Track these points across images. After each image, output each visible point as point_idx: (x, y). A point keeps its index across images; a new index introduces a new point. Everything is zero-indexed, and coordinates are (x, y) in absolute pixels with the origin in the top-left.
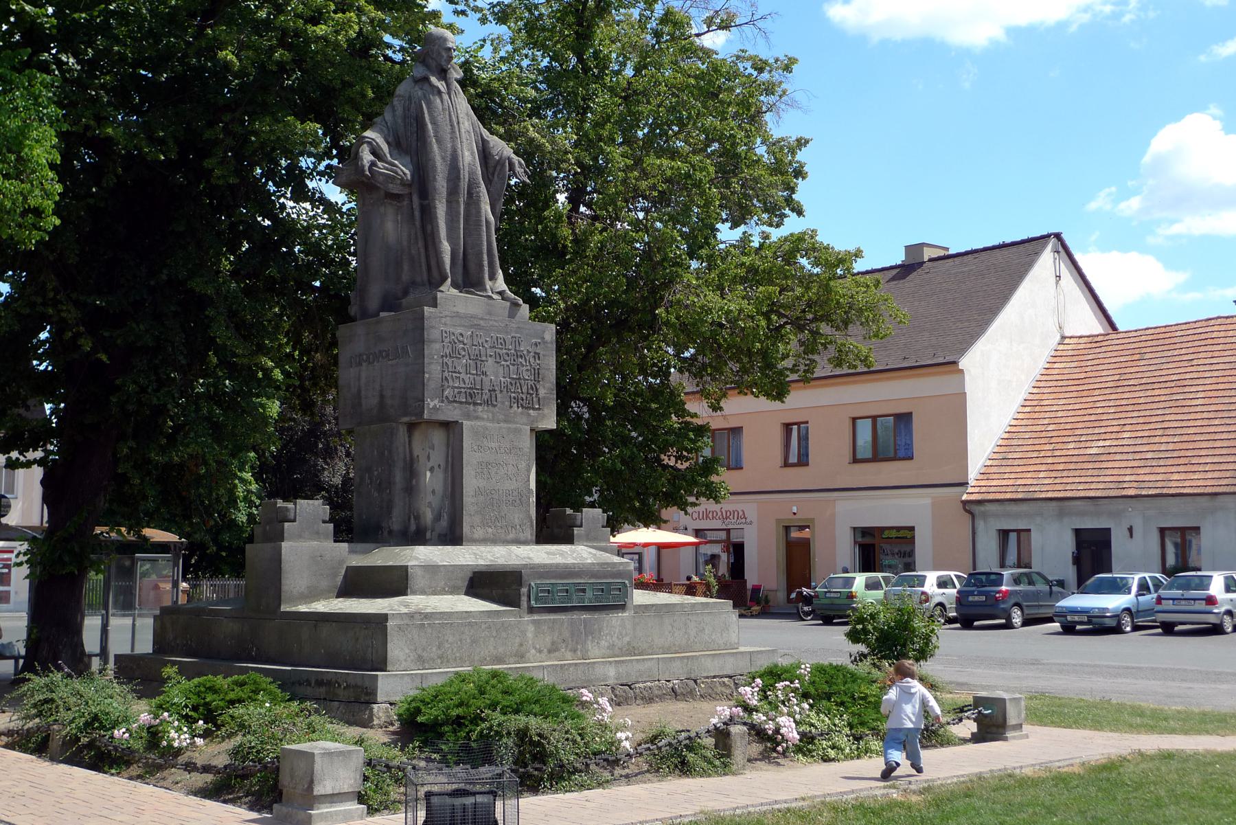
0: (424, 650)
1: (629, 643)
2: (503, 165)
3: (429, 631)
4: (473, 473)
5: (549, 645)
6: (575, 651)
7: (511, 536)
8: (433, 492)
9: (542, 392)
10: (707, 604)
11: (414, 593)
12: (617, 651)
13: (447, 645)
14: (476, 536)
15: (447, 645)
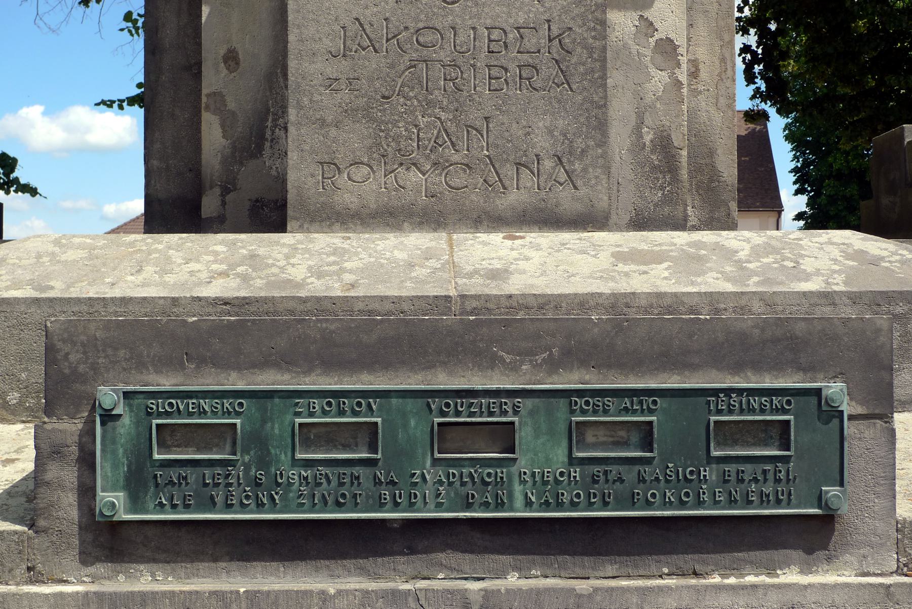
7: (514, 198)
8: (231, 59)
14: (347, 198)
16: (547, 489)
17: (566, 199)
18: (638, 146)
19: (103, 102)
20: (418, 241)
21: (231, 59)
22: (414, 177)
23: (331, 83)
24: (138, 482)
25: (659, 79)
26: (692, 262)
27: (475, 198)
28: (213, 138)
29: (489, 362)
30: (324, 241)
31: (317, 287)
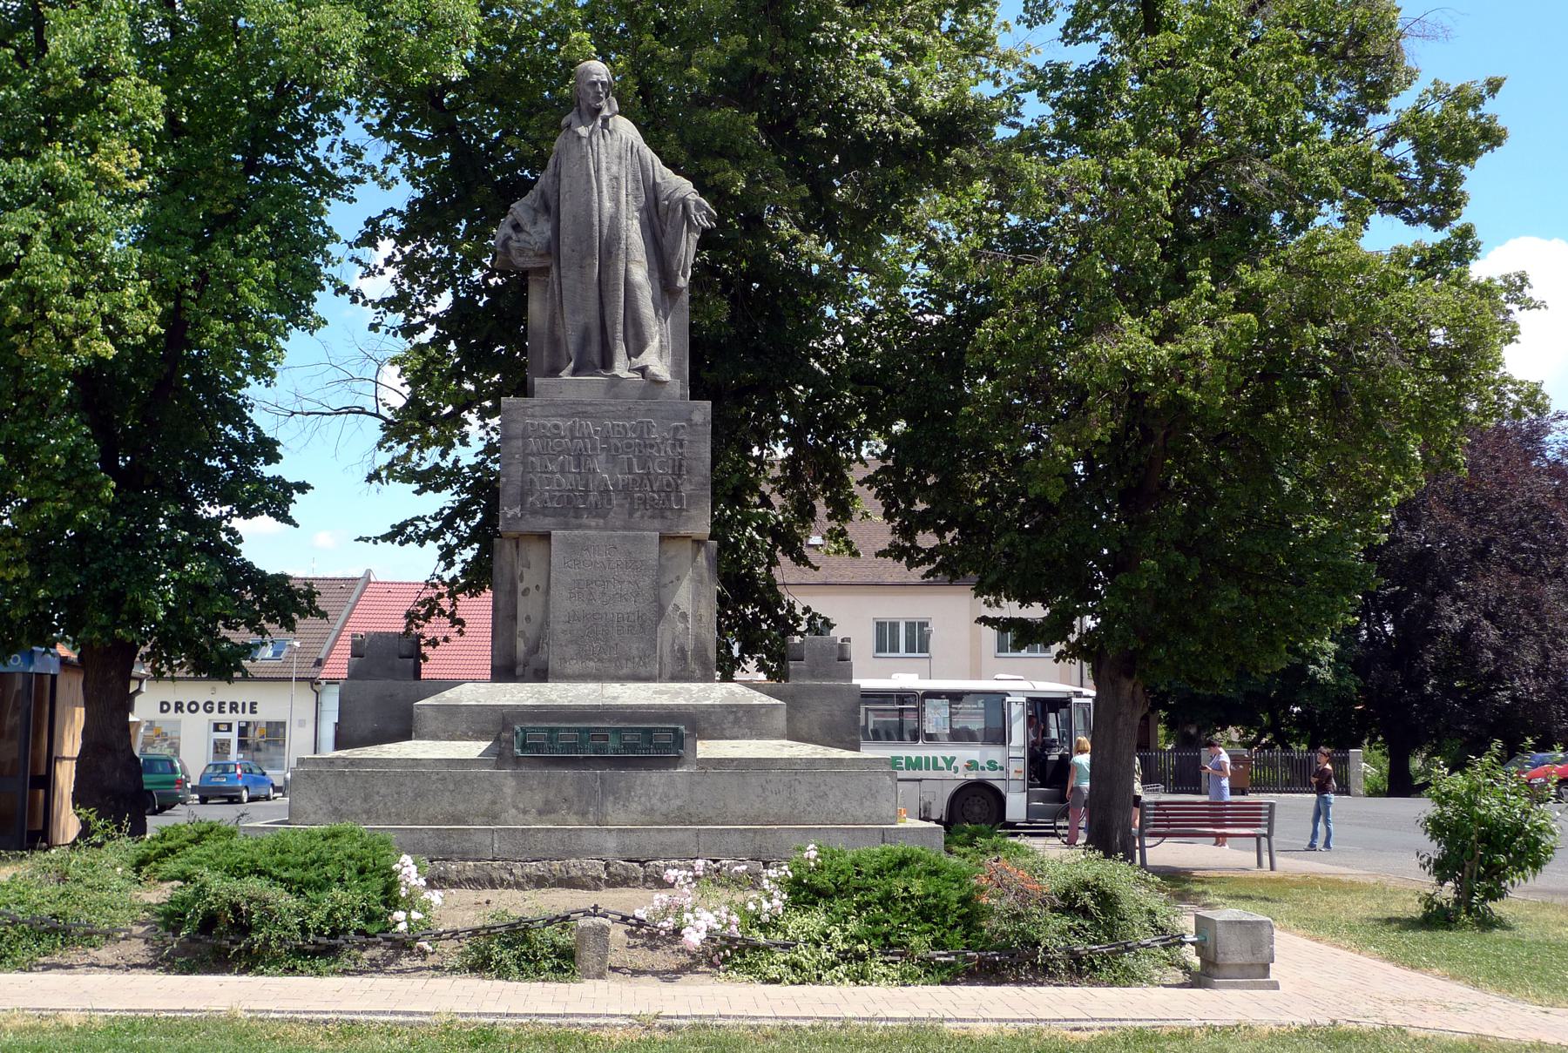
0: (342, 802)
1: (680, 808)
2: (675, 210)
3: (351, 780)
4: (566, 594)
5: (540, 805)
6: (584, 814)
7: (625, 671)
8: (528, 618)
9: (686, 489)
10: (840, 761)
11: (421, 737)
12: (658, 817)
13: (377, 798)
14: (569, 671)
15: (377, 798)
16: (616, 751)
17: (643, 671)
18: (672, 651)
19: (361, 539)
20: (592, 686)
21: (528, 618)
22: (591, 664)
23: (564, 632)
24: (524, 747)
25: (681, 626)
26: (678, 694)
27: (612, 671)
28: (521, 647)
29: (602, 720)
30: (562, 686)
31: (560, 702)
